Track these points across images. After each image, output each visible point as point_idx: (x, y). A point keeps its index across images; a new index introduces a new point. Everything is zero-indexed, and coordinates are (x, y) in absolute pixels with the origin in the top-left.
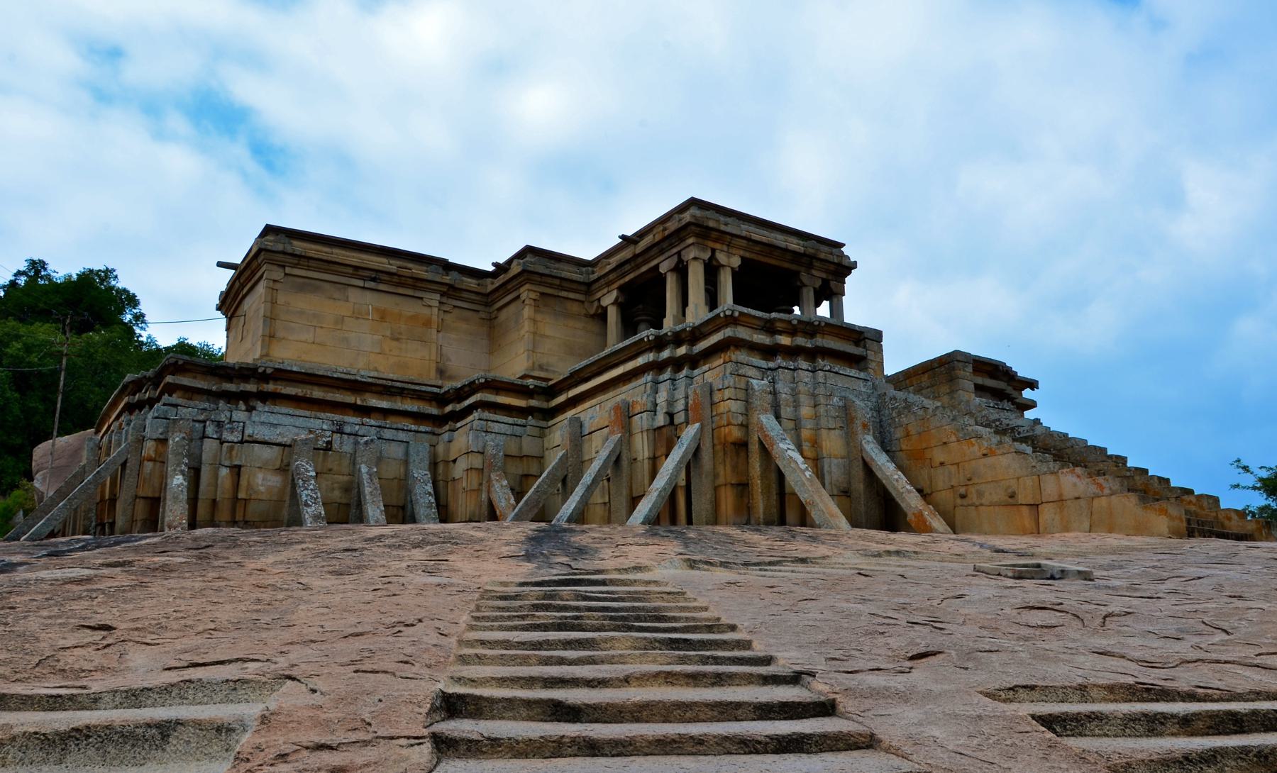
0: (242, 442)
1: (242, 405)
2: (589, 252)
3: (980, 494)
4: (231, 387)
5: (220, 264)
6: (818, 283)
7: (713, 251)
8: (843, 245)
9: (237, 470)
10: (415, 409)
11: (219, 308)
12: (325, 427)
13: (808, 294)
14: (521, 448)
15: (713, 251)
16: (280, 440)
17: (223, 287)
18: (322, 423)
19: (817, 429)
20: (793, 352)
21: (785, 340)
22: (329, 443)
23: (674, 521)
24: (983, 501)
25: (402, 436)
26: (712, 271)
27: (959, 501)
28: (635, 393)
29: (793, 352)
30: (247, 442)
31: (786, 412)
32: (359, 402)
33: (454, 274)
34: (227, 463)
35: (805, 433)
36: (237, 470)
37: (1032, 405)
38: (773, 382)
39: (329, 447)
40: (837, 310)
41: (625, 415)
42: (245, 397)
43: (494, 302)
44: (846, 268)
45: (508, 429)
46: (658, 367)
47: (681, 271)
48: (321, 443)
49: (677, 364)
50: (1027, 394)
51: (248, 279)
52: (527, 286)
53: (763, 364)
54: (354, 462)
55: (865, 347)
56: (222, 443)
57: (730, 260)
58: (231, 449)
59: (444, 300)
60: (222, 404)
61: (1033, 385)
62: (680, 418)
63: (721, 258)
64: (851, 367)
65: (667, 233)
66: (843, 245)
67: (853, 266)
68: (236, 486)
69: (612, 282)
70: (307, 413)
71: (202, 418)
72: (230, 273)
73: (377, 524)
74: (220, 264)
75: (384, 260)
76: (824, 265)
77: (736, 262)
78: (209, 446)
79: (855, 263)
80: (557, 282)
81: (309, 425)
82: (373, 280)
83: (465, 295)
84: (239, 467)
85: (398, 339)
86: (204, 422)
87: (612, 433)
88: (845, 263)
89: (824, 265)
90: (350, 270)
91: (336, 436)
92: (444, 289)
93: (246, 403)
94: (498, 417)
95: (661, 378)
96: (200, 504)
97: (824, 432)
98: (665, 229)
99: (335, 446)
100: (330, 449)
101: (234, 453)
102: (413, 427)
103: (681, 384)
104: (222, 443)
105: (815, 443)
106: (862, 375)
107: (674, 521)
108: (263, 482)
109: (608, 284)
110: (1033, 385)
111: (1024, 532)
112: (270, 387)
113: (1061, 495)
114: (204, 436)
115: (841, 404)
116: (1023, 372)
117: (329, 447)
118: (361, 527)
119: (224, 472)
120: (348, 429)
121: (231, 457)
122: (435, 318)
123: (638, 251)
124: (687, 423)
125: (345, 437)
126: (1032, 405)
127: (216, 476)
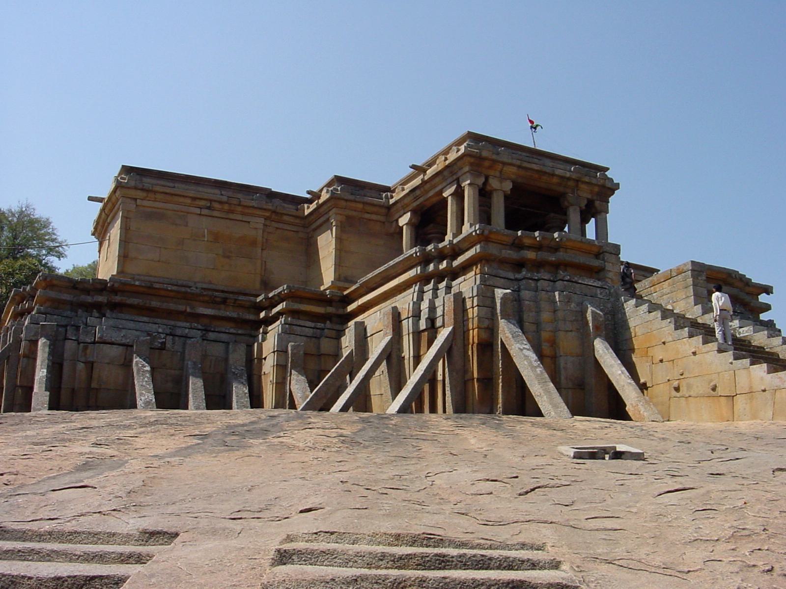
0: (94, 343)
1: (95, 313)
2: (610, 199)
3: (689, 387)
4: (89, 299)
5: (91, 199)
6: (583, 204)
7: (487, 178)
8: (607, 169)
9: (90, 366)
10: (235, 315)
11: (93, 234)
12: (160, 330)
13: (574, 216)
14: (319, 348)
15: (487, 178)
16: (124, 341)
17: (95, 216)
18: (159, 327)
19: (556, 331)
20: (539, 265)
21: (531, 255)
22: (164, 343)
23: (420, 410)
24: (692, 393)
25: (224, 337)
26: (484, 194)
27: (674, 393)
28: (404, 302)
29: (539, 265)
30: (98, 342)
31: (529, 317)
32: (188, 310)
33: (277, 202)
34: (83, 359)
35: (545, 335)
36: (90, 366)
37: (767, 308)
38: (517, 291)
39: (163, 347)
40: (601, 230)
41: (396, 318)
42: (98, 306)
43: (310, 224)
44: (610, 189)
45: (309, 332)
46: (424, 279)
47: (459, 195)
48: (157, 344)
49: (439, 277)
50: (763, 298)
51: (111, 210)
52: (334, 210)
53: (511, 275)
54: (183, 359)
55: (603, 260)
56: (79, 343)
57: (501, 187)
58: (85, 348)
59: (268, 223)
60: (80, 311)
61: (768, 290)
62: (439, 323)
63: (494, 183)
64: (591, 277)
65: (447, 162)
66: (607, 169)
67: (617, 186)
68: (90, 377)
69: (407, 205)
70: (145, 319)
71: (64, 323)
72: (100, 205)
73: (192, 410)
74: (91, 199)
75: (217, 191)
76: (590, 190)
77: (508, 186)
78: (70, 346)
79: (618, 184)
80: (360, 206)
81: (148, 329)
82: (209, 208)
83: (285, 218)
84: (92, 363)
85: (229, 257)
86: (66, 326)
87: (386, 335)
88: (608, 185)
89: (590, 190)
90: (188, 201)
91: (170, 338)
92: (268, 214)
93: (99, 311)
94: (302, 323)
95: (426, 288)
96: (63, 392)
97: (561, 334)
98: (446, 159)
99: (168, 345)
100: (164, 349)
101: (88, 351)
102: (232, 331)
103: (441, 292)
104: (79, 343)
105: (553, 343)
106: (599, 284)
107: (420, 410)
108: (108, 375)
109: (403, 207)
110: (768, 290)
111: (722, 419)
112: (118, 299)
113: (751, 387)
114: (66, 339)
115: (578, 309)
116: (757, 279)
117: (163, 347)
118: (134, 411)
119: (81, 366)
120: (179, 332)
121: (86, 354)
122: (260, 239)
123: (426, 178)
124: (443, 326)
125: (177, 338)
126: (767, 308)
127: (74, 370)
